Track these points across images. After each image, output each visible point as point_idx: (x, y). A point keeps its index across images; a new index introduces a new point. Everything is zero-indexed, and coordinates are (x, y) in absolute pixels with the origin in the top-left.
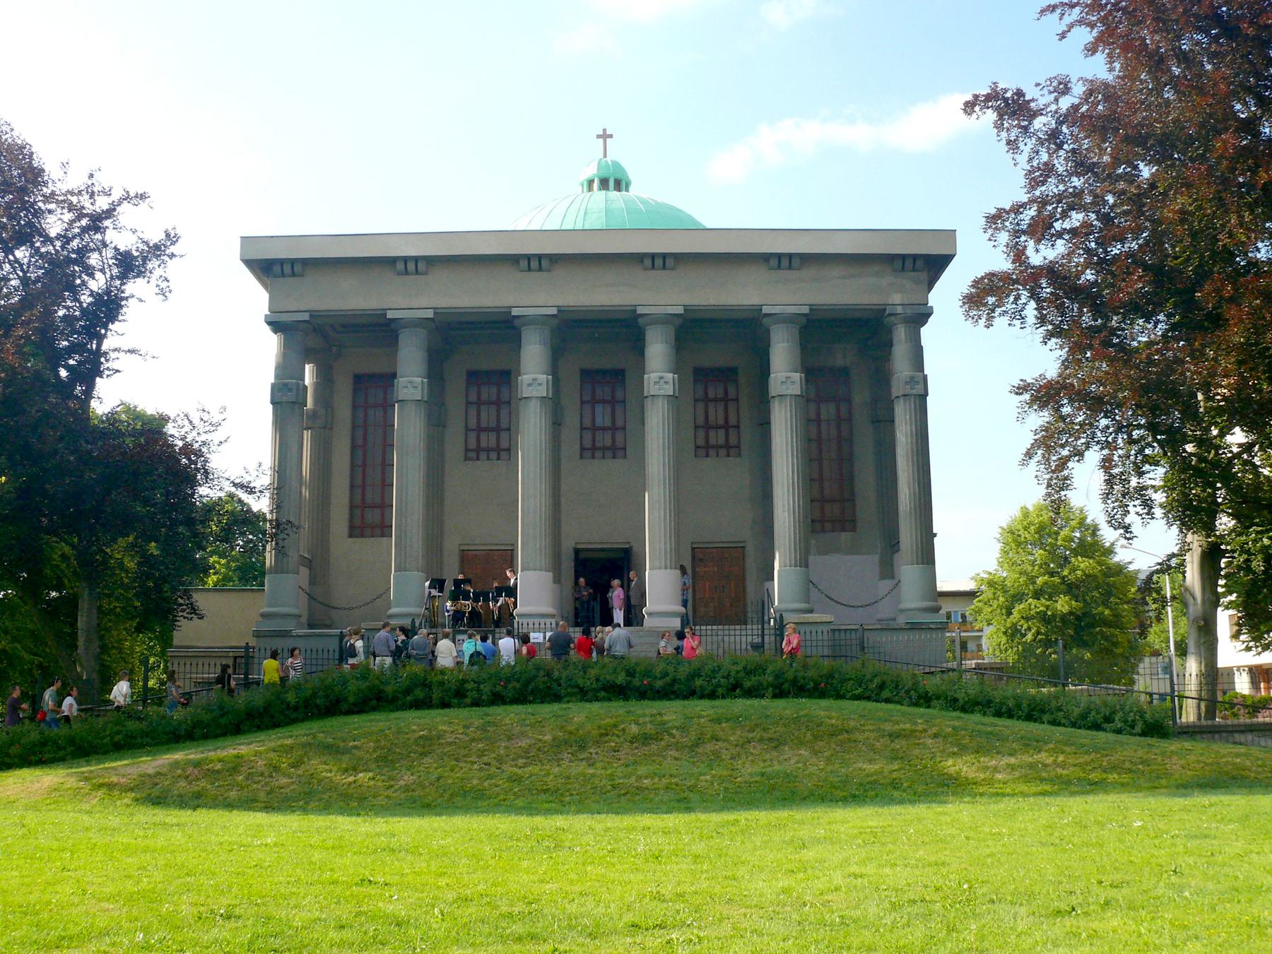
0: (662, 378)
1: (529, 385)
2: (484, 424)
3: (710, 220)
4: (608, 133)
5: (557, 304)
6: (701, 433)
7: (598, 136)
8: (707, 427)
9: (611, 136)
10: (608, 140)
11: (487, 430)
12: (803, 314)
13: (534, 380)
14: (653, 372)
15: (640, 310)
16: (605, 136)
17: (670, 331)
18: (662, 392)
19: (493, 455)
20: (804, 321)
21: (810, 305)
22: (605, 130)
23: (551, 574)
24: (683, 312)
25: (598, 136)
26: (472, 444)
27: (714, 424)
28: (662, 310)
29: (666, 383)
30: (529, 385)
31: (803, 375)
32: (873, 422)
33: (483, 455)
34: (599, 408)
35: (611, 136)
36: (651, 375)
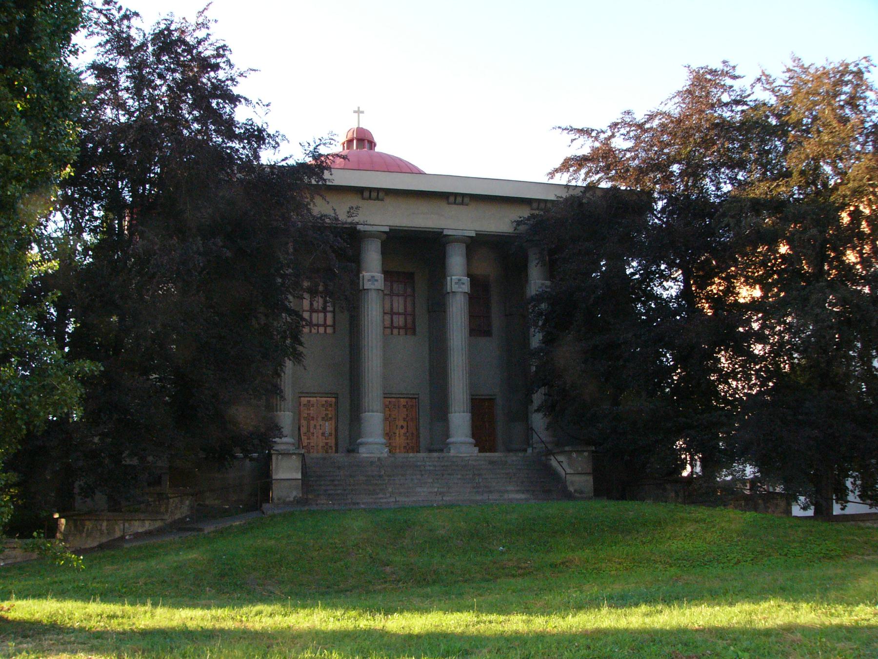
0: (460, 280)
1: (369, 280)
2: (395, 310)
3: (428, 168)
4: (357, 110)
5: (388, 224)
6: (388, 318)
7: (355, 112)
8: (392, 313)
9: (362, 112)
10: (361, 115)
11: (317, 311)
12: (384, 232)
13: (460, 280)
14: (455, 276)
15: (446, 232)
16: (358, 112)
17: (384, 245)
18: (460, 290)
19: (402, 332)
20: (385, 236)
21: (390, 226)
22: (359, 108)
23: (470, 414)
24: (388, 230)
25: (355, 112)
26: (388, 323)
27: (316, 309)
28: (460, 233)
29: (463, 284)
30: (369, 280)
31: (469, 279)
32: (506, 315)
33: (395, 331)
34: (395, 299)
35: (362, 112)
36: (453, 277)
